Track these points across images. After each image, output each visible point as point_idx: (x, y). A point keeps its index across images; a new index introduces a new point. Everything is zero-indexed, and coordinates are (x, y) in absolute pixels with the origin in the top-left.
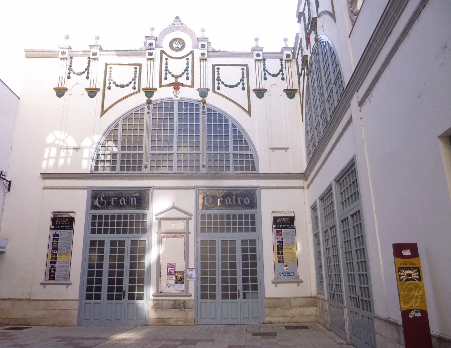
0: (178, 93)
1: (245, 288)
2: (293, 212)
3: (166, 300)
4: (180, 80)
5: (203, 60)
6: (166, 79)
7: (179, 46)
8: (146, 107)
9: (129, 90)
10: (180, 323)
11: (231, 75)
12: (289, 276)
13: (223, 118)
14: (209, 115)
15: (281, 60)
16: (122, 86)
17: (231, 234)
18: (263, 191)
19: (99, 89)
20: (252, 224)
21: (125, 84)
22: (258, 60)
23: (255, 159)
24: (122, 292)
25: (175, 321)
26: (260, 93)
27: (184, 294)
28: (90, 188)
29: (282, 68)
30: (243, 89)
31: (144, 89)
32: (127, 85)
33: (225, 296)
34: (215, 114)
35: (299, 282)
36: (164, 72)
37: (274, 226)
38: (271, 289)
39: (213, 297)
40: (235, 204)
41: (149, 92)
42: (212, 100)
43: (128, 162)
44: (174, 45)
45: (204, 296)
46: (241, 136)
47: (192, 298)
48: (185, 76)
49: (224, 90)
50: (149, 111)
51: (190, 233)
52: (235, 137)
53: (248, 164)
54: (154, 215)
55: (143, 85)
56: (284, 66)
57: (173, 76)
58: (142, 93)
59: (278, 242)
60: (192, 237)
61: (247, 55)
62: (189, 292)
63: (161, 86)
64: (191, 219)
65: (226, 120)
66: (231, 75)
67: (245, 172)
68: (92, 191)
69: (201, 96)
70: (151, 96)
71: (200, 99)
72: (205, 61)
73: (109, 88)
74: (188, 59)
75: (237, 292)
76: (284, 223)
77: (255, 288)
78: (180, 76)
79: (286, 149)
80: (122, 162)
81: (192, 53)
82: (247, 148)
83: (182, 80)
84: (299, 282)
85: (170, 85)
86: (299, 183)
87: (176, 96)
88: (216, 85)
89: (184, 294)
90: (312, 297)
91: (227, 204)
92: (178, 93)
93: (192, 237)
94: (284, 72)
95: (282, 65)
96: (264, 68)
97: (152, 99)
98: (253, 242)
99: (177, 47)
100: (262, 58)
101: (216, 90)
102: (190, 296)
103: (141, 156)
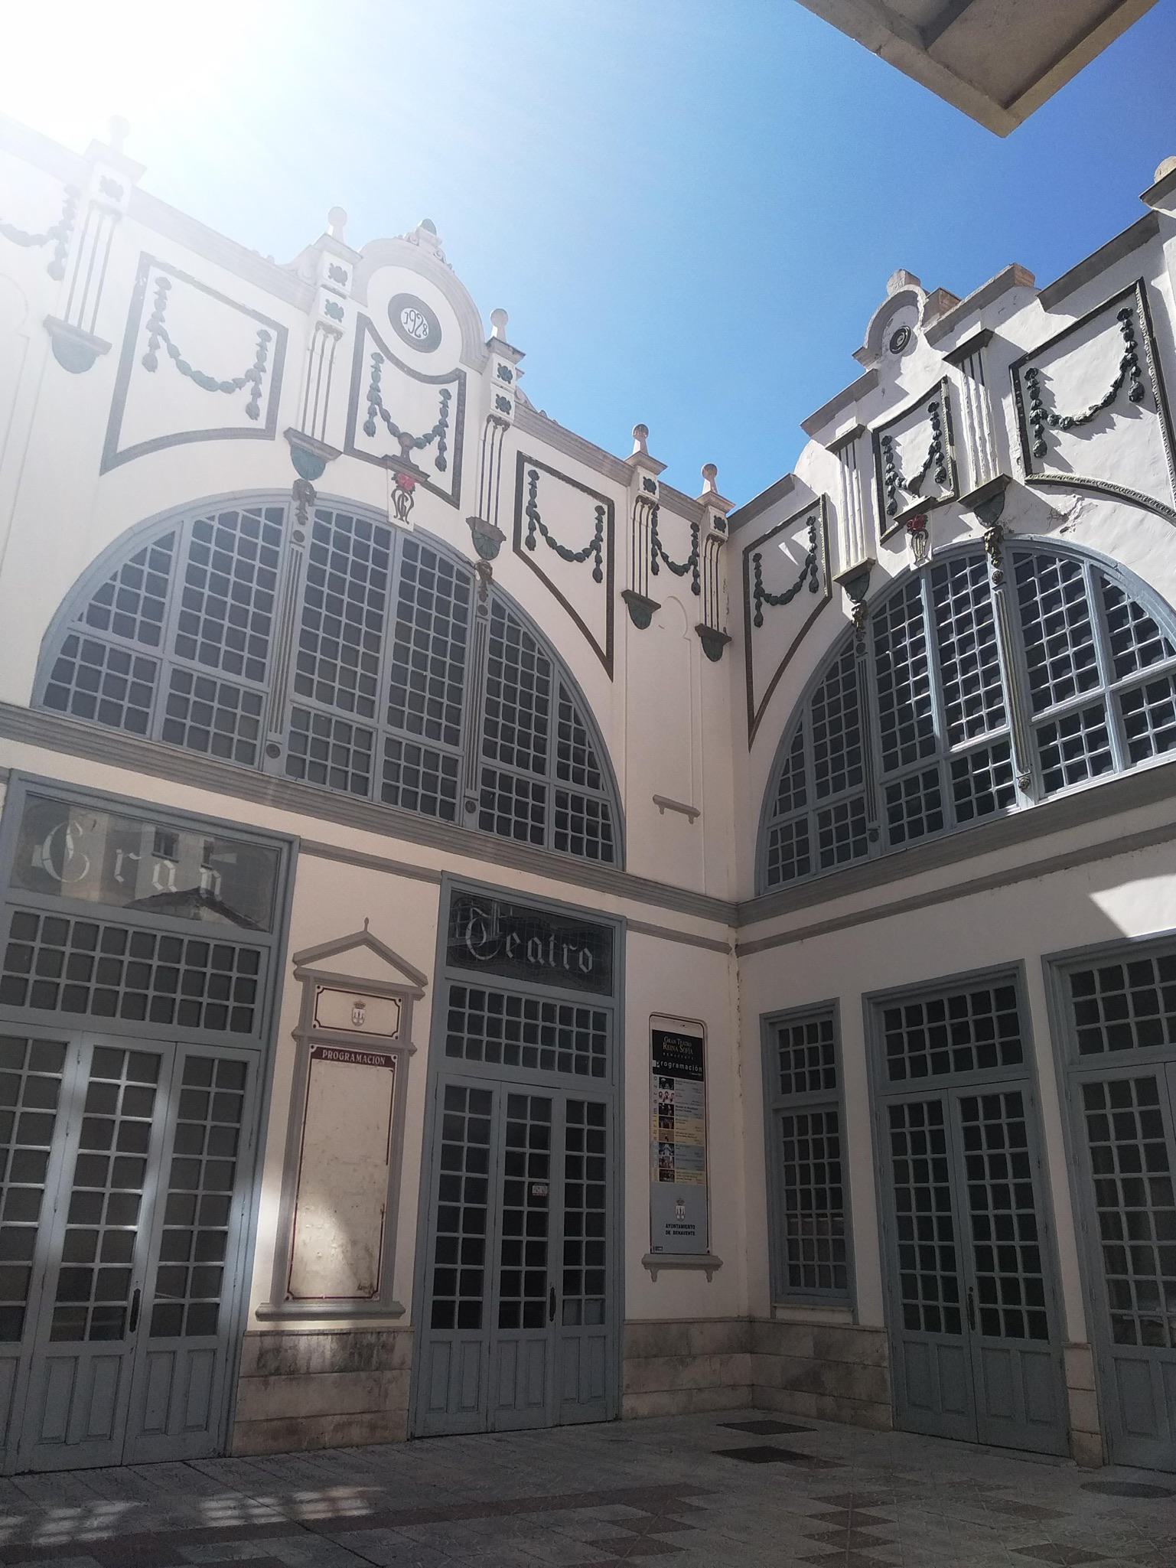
0: (407, 504)
1: (571, 1282)
2: (701, 1024)
3: (311, 1334)
4: (417, 457)
5: (498, 421)
6: (370, 430)
7: (420, 331)
8: (291, 509)
9: (231, 411)
10: (357, 1434)
11: (569, 518)
12: (685, 1243)
13: (537, 655)
14: (497, 628)
15: (695, 527)
16: (207, 383)
17: (537, 1074)
18: (631, 936)
19: (106, 347)
20: (590, 1045)
21: (219, 379)
22: (644, 500)
23: (613, 822)
24: (125, 1298)
25: (339, 1427)
26: (642, 610)
27: (375, 1305)
28: (26, 778)
29: (695, 554)
30: (597, 576)
31: (289, 433)
32: (228, 388)
33: (508, 1318)
34: (514, 634)
35: (711, 1266)
36: (364, 405)
37: (654, 1063)
38: (646, 1294)
39: (471, 1317)
40: (553, 964)
41: (310, 457)
42: (508, 572)
43: (203, 713)
44: (403, 318)
45: (441, 1317)
46: (580, 737)
47: (405, 1321)
48: (432, 450)
49: (543, 555)
50: (301, 528)
51: (412, 1052)
52: (563, 732)
53: (589, 831)
54: (290, 957)
55: (287, 418)
56: (701, 550)
57: (393, 430)
58: (279, 452)
59: (841, 1215)
60: (418, 1067)
61: (623, 472)
62: (396, 1297)
63: (350, 449)
64: (420, 996)
65: (544, 667)
66: (569, 518)
67: (94, 725)
68: (30, 795)
69: (479, 550)
70: (318, 473)
71: (474, 557)
72: (500, 428)
73: (150, 364)
74: (446, 394)
75: (547, 1299)
76: (679, 1056)
77: (597, 1283)
78: (420, 444)
79: (692, 813)
80: (177, 705)
81: (459, 377)
82: (594, 783)
83: (423, 459)
84: (711, 1266)
85: (384, 461)
86: (717, 930)
87: (402, 513)
88: (525, 532)
89: (375, 1305)
90: (738, 1320)
91: (532, 959)
92: (407, 504)
93: (418, 1067)
94: (700, 568)
95: (695, 544)
96: (655, 533)
97: (318, 485)
98: (597, 1112)
99: (415, 331)
100: (656, 499)
101: (524, 548)
102: (398, 1314)
103: (254, 702)
